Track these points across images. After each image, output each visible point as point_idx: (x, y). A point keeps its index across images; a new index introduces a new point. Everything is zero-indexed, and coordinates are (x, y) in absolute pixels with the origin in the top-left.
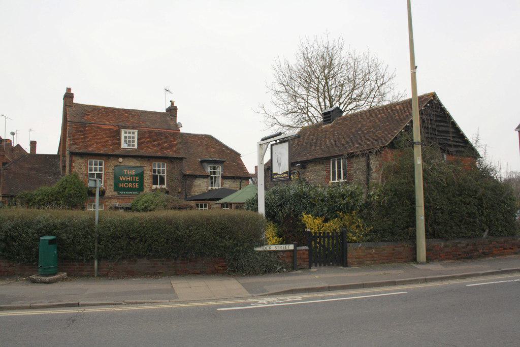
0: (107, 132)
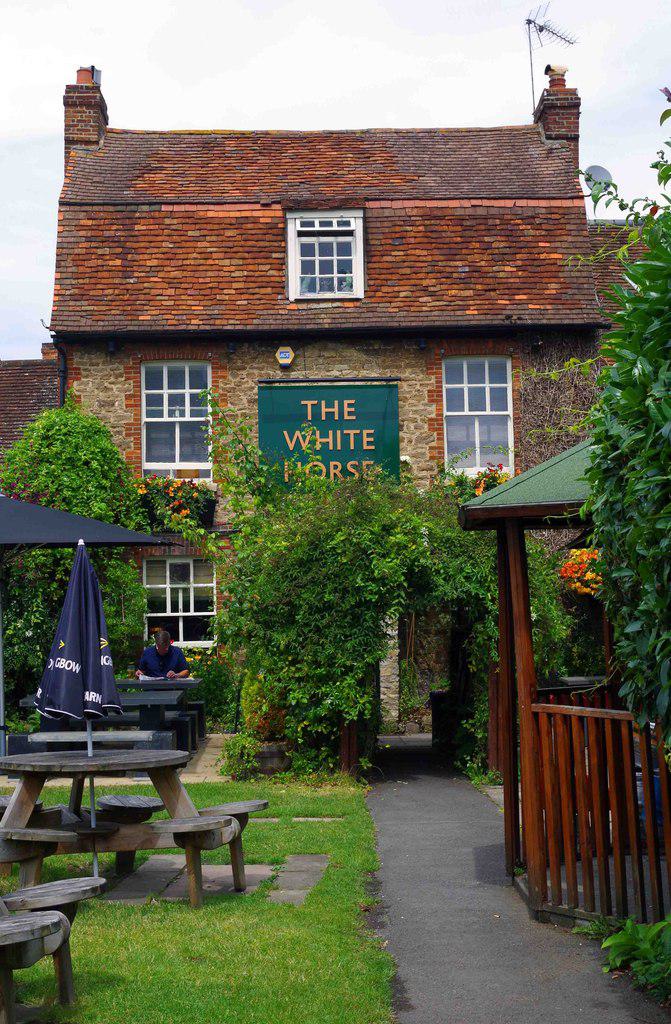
0: (229, 233)
